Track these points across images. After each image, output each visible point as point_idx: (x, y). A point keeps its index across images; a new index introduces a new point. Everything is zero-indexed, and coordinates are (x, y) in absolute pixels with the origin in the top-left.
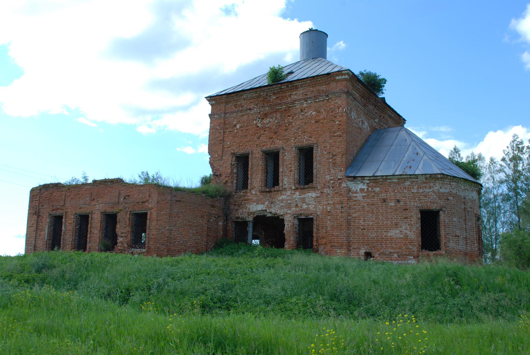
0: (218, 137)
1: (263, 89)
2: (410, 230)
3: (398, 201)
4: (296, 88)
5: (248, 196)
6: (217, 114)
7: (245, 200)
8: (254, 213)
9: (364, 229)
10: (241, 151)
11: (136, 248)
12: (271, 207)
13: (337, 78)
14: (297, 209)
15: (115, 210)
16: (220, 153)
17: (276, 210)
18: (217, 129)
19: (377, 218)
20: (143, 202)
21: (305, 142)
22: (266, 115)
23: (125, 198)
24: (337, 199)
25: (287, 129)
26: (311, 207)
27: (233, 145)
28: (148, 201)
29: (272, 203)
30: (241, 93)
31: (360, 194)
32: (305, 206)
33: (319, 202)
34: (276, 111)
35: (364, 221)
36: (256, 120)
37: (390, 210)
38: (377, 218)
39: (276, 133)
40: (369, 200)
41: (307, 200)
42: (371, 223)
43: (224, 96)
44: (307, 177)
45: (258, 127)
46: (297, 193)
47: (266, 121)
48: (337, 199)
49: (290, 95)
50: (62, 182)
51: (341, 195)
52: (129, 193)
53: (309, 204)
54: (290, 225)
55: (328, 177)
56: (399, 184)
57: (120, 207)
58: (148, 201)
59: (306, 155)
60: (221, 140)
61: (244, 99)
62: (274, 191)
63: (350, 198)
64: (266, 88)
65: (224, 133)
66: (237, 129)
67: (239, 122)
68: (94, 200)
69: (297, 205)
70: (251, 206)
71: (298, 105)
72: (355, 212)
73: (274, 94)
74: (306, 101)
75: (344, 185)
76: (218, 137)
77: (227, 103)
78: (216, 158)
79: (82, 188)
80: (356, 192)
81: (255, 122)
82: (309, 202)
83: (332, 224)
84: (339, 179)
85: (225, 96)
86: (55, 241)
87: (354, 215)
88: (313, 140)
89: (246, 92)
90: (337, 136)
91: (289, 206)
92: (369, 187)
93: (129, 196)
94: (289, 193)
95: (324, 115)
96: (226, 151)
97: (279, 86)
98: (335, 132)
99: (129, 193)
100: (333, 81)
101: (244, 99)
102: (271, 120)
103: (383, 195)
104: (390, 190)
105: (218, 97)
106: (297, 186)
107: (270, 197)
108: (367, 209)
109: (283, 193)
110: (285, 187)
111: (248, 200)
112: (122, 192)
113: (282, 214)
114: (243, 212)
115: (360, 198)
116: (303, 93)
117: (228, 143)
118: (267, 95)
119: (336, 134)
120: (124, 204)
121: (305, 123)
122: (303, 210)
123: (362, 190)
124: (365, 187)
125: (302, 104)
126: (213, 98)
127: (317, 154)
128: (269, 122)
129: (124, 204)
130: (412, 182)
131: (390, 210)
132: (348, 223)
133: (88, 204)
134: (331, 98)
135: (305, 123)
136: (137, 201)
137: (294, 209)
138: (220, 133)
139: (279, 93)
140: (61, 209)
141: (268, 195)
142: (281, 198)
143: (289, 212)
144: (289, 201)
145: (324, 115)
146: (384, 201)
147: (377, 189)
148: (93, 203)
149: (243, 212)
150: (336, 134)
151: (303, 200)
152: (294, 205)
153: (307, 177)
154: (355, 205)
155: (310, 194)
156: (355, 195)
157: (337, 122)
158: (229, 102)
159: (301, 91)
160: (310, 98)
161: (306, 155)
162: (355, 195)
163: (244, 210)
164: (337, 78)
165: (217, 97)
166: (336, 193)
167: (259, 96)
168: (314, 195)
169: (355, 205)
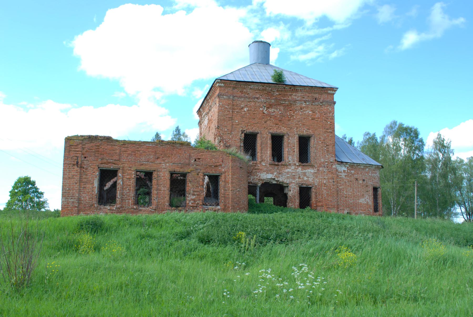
0: (227, 115)
1: (271, 85)
2: (367, 200)
3: (364, 180)
4: (297, 91)
5: (258, 166)
6: (226, 95)
7: (255, 169)
8: (264, 180)
9: (346, 197)
10: (250, 130)
11: (206, 205)
12: (279, 177)
13: (329, 92)
14: (300, 180)
15: (186, 170)
16: (229, 127)
17: (282, 179)
18: (226, 108)
19: (353, 190)
20: (216, 166)
21: (305, 132)
22: (270, 106)
23: (195, 160)
24: (330, 176)
25: (290, 120)
26: (310, 180)
27: (241, 124)
28: (221, 165)
29: (280, 174)
30: (250, 84)
31: (344, 174)
32: (305, 179)
33: (317, 177)
34: (281, 104)
35: (346, 192)
36: (262, 108)
37: (360, 186)
38: (353, 190)
39: (280, 121)
40: (348, 178)
41: (307, 174)
42: (350, 193)
43: (234, 82)
44: (304, 157)
45: (264, 113)
46: (300, 168)
47: (271, 110)
48: (330, 176)
49: (291, 95)
50: (115, 137)
51: (332, 173)
52: (200, 156)
53: (308, 177)
54: (293, 192)
55: (322, 160)
56: (363, 169)
57: (191, 168)
58: (221, 165)
59: (304, 142)
60: (230, 118)
61: (251, 89)
62: (282, 165)
63: (338, 176)
64: (273, 85)
65: (232, 112)
66: (244, 111)
67: (246, 106)
68: (158, 158)
69: (300, 177)
70: (262, 175)
71: (298, 104)
72: (341, 186)
73: (278, 91)
74: (305, 102)
75: (334, 167)
76: (227, 115)
77: (234, 88)
78: (225, 131)
79: (142, 146)
80: (341, 172)
81: (261, 109)
82: (309, 176)
83: (327, 192)
84: (331, 162)
85: (235, 82)
86: (107, 197)
87: (340, 188)
88: (310, 132)
89: (254, 84)
90: (329, 132)
91: (294, 177)
92: (348, 169)
93: (199, 159)
94: (293, 167)
95: (318, 115)
96: (235, 127)
97: (284, 86)
98: (328, 129)
99: (200, 156)
100: (326, 93)
101: (251, 89)
102: (275, 110)
103: (356, 176)
104: (360, 173)
105: (229, 82)
106: (300, 163)
107: (278, 169)
108: (348, 184)
109: (290, 167)
110: (290, 163)
111: (258, 169)
112: (192, 155)
113: (288, 182)
114: (254, 179)
115: (344, 177)
116: (301, 96)
117: (237, 121)
118: (271, 90)
119: (328, 131)
120: (195, 166)
121: (304, 119)
122: (304, 181)
123: (344, 171)
124: (346, 169)
125: (302, 104)
126: (223, 81)
127: (312, 143)
128: (274, 112)
129: (195, 166)
130: (369, 169)
131: (360, 186)
132: (337, 191)
133: (152, 162)
134: (324, 105)
135: (304, 119)
136: (210, 165)
137: (297, 179)
138: (229, 111)
139: (282, 91)
140: (115, 164)
141: (276, 167)
142: (287, 171)
143: (293, 181)
144: (293, 174)
145: (318, 115)
146: (357, 179)
147: (353, 172)
148: (158, 161)
149: (254, 179)
150: (328, 131)
151: (305, 174)
152: (298, 177)
153: (304, 157)
154: (340, 180)
155: (309, 170)
156: (340, 174)
157: (329, 123)
158: (236, 88)
159: (299, 94)
160: (308, 101)
161: (304, 142)
162: (340, 174)
163: (255, 177)
164: (329, 92)
165: (228, 82)
166: (329, 172)
167: (265, 90)
168: (312, 171)
169: (340, 180)
